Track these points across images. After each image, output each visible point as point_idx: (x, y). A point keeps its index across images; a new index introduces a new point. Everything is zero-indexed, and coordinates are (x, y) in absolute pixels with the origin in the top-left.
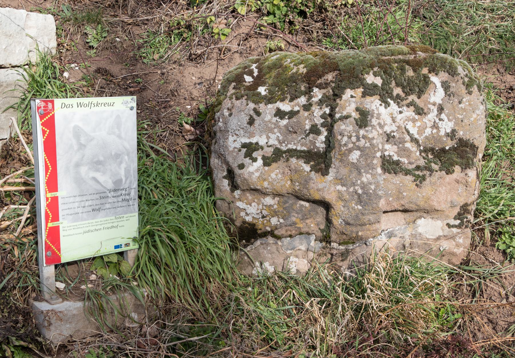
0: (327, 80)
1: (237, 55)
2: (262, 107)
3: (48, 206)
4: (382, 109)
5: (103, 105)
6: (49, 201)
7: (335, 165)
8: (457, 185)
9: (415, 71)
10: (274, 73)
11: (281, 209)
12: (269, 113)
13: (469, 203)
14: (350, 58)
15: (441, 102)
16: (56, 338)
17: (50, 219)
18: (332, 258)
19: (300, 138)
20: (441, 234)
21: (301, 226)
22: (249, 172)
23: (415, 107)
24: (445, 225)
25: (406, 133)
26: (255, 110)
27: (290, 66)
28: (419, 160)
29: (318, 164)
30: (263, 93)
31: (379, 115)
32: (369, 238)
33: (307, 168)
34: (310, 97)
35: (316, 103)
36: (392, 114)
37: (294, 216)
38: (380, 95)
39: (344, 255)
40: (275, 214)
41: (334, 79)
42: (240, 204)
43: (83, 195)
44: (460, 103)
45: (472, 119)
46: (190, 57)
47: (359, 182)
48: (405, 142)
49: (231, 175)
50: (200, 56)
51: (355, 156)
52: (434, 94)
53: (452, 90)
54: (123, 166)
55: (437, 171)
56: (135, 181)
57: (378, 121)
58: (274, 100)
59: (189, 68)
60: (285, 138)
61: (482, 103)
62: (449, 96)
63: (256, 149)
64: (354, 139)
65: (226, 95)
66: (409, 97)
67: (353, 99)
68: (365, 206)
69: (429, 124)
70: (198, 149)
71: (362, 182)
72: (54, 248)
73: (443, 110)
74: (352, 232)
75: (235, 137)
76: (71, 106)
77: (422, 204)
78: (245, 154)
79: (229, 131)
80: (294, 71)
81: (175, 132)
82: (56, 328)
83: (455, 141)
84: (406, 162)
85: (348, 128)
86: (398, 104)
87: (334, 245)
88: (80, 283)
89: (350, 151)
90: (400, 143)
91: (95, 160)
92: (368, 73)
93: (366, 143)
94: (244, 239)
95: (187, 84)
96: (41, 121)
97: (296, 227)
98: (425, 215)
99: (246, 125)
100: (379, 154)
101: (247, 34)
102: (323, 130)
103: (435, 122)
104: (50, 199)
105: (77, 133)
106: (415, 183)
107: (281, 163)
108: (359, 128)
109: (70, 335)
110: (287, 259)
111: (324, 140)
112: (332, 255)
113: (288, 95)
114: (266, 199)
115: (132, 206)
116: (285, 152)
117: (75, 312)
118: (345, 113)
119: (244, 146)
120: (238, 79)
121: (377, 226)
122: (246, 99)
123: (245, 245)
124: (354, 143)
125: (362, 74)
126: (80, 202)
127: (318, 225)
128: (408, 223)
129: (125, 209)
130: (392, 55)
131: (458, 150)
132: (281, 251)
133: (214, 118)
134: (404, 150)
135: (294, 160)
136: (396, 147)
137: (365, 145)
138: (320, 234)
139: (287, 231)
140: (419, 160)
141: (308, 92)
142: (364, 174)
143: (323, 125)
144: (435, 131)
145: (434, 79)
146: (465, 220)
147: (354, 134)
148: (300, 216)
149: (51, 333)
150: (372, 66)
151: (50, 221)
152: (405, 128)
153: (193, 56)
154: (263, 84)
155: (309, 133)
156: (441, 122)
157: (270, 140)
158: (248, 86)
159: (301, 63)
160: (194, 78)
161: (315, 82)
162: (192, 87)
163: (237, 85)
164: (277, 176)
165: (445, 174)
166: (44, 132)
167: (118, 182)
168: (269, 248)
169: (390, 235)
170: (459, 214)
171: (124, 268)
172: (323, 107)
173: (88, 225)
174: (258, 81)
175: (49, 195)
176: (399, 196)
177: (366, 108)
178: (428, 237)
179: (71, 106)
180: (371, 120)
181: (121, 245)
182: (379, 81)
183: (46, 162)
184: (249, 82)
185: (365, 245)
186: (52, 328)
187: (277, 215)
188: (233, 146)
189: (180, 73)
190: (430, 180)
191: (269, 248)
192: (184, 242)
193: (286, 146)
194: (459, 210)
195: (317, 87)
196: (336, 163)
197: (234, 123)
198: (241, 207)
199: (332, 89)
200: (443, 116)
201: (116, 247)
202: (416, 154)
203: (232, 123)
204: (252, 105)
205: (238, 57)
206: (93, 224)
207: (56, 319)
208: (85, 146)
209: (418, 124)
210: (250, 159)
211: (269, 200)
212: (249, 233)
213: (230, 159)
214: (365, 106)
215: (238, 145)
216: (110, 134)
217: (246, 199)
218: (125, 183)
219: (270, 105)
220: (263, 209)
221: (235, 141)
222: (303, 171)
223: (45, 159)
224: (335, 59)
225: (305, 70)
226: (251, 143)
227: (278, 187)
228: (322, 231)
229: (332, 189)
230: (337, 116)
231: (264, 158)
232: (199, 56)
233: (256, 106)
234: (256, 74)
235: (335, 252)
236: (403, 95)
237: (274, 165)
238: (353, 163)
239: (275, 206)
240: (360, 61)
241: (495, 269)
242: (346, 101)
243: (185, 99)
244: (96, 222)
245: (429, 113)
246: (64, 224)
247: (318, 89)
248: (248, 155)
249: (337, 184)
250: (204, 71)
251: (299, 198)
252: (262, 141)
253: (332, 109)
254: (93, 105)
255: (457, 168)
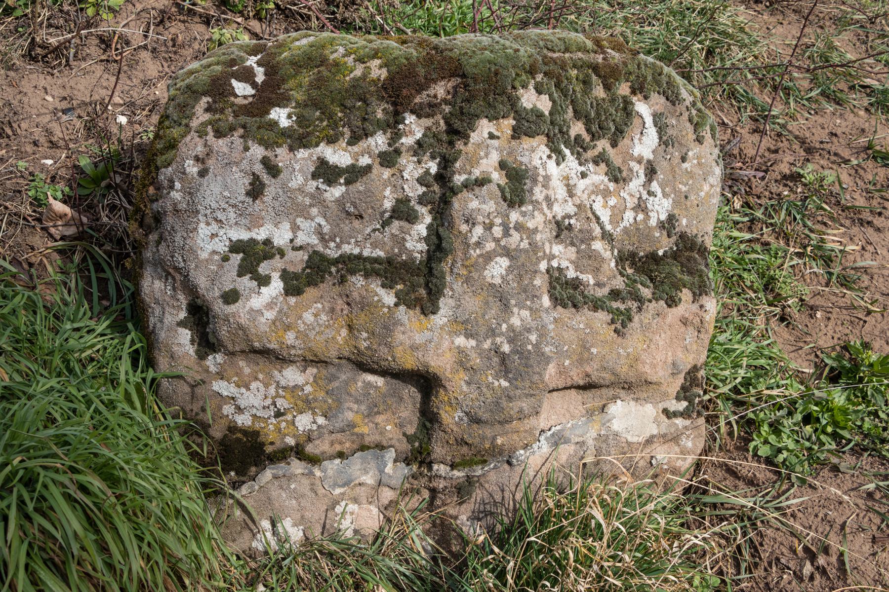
0: (435, 96)
1: (145, 55)
2: (282, 155)
4: (551, 164)
7: (452, 289)
8: (683, 329)
9: (607, 87)
10: (306, 78)
11: (321, 395)
12: (300, 171)
13: (699, 365)
14: (486, 49)
15: (651, 157)
18: (433, 498)
19: (369, 230)
20: (655, 432)
21: (365, 430)
22: (252, 310)
23: (608, 165)
24: (660, 411)
25: (594, 219)
26: (265, 162)
27: (346, 63)
28: (615, 277)
29: (413, 288)
30: (284, 123)
31: (547, 178)
32: (516, 449)
33: (389, 298)
34: (396, 136)
35: (410, 148)
36: (567, 178)
37: (350, 409)
38: (547, 135)
39: (463, 491)
40: (307, 405)
41: (450, 97)
42: (222, 387)
44: (684, 159)
45: (702, 194)
46: (30, 51)
47: (504, 326)
48: (593, 239)
49: (199, 316)
50: (58, 51)
51: (498, 269)
52: (640, 139)
53: (670, 132)
55: (650, 301)
57: (545, 191)
58: (314, 140)
59: (31, 76)
60: (336, 230)
61: (717, 162)
62: (666, 144)
63: (268, 256)
64: (497, 231)
65: (187, 125)
66: (598, 143)
67: (495, 142)
68: (516, 380)
69: (631, 202)
70: (84, 260)
71: (511, 328)
73: (655, 173)
74: (483, 438)
75: (214, 227)
77: (623, 370)
78: (240, 266)
79: (198, 212)
80: (358, 72)
81: (24, 219)
83: (674, 238)
84: (592, 282)
85: (484, 206)
86: (579, 156)
87: (441, 469)
89: (488, 258)
90: (582, 242)
92: (525, 86)
93: (522, 240)
94: (232, 470)
95: (34, 111)
97: (352, 434)
98: (622, 393)
99: (242, 198)
100: (543, 266)
101: (163, 12)
102: (423, 210)
103: (640, 198)
106: (613, 327)
107: (327, 287)
108: (509, 206)
110: (333, 509)
111: (424, 233)
112: (433, 492)
113: (346, 129)
114: (285, 372)
116: (336, 262)
118: (477, 173)
119: (236, 247)
120: (219, 90)
121: (533, 421)
122: (242, 137)
123: (234, 483)
124: (497, 241)
125: (514, 87)
127: (401, 426)
128: (590, 413)
130: (567, 50)
131: (680, 256)
132: (321, 491)
133: (154, 182)
134: (590, 257)
135: (358, 281)
136: (574, 249)
137: (519, 245)
138: (405, 446)
139: (332, 444)
140: (615, 277)
141: (393, 125)
142: (515, 310)
143: (421, 200)
144: (640, 217)
145: (642, 108)
146: (697, 400)
147: (498, 221)
148: (363, 408)
150: (532, 72)
152: (591, 208)
153: (39, 50)
154: (282, 101)
155: (391, 217)
156: (651, 198)
157: (300, 234)
158: (241, 107)
159: (375, 56)
160: (49, 98)
161: (410, 97)
162: (48, 118)
163: (215, 102)
164: (316, 318)
165: (665, 305)
168: (293, 486)
169: (558, 441)
170: (683, 388)
172: (425, 158)
174: (270, 94)
176: (583, 355)
177: (521, 163)
178: (630, 439)
180: (532, 189)
182: (544, 104)
184: (245, 97)
185: (506, 466)
187: (310, 408)
188: (210, 248)
189: (11, 85)
190: (641, 320)
191: (293, 486)
192: (118, 492)
193: (338, 247)
194: (683, 381)
195: (413, 112)
196: (455, 287)
197: (212, 191)
198: (225, 393)
199: (443, 118)
200: (655, 186)
202: (609, 265)
203: (208, 192)
204: (258, 151)
205: (149, 59)
209: (612, 201)
210: (251, 279)
211: (292, 376)
212: (244, 453)
213: (201, 281)
214: (519, 158)
215: (222, 247)
217: (237, 374)
219: (302, 150)
220: (278, 396)
221: (213, 236)
222: (380, 304)
224: (451, 50)
225: (384, 73)
226: (253, 241)
227: (318, 342)
228: (409, 439)
229: (446, 344)
230: (459, 179)
231: (285, 276)
232: (53, 52)
233: (269, 154)
234: (260, 78)
235: (441, 484)
236: (587, 138)
237: (311, 293)
238: (492, 285)
239: (308, 389)
240: (507, 57)
241: (768, 498)
242: (479, 145)
243: (35, 143)
245: (631, 180)
247: (414, 117)
248: (249, 268)
249: (457, 334)
250: (72, 83)
251: (363, 367)
252: (281, 236)
253: (446, 163)
255: (686, 295)
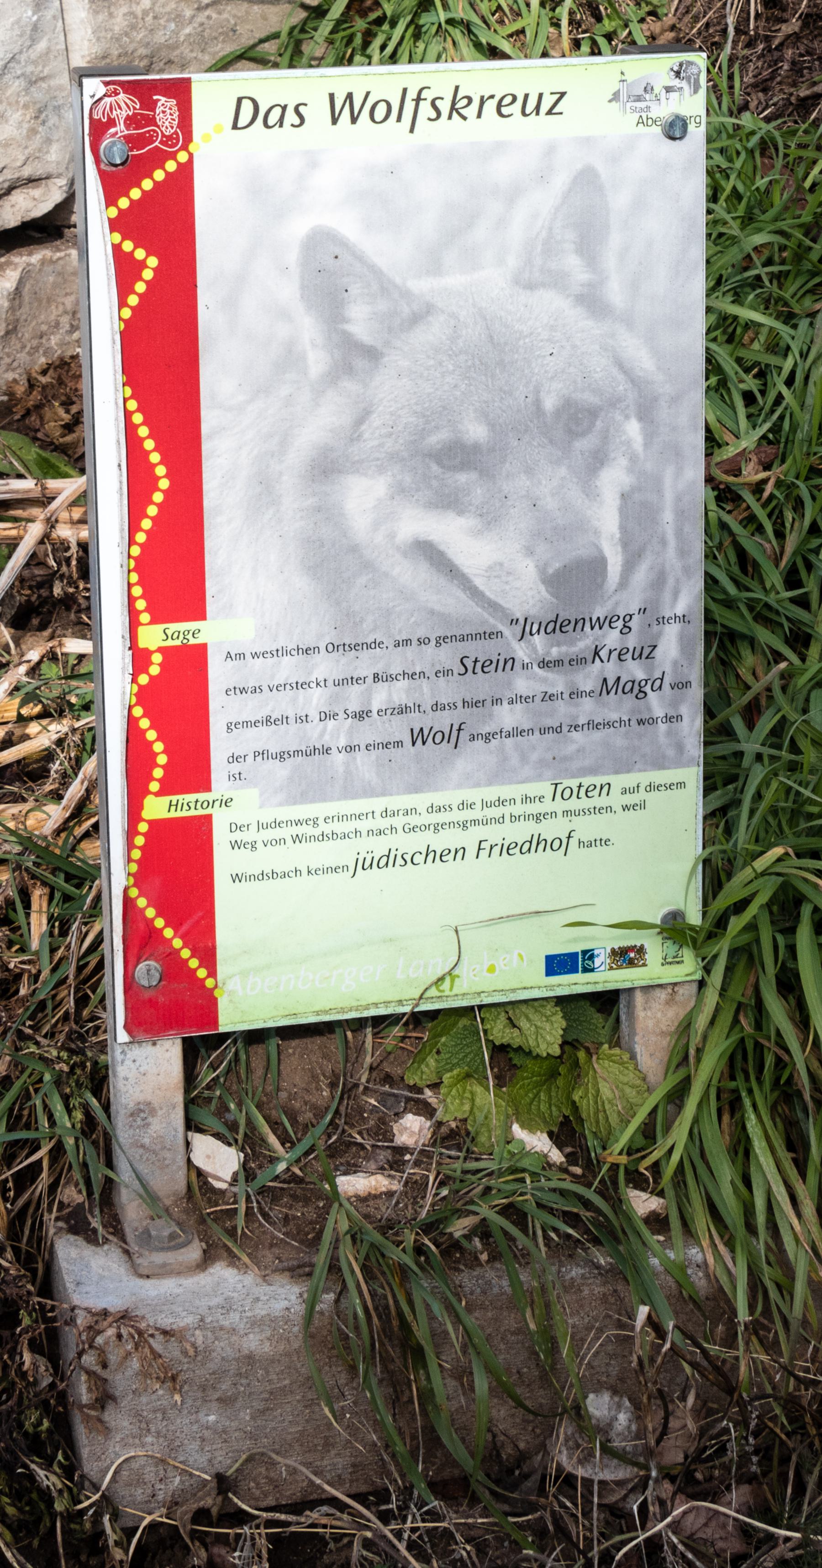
3: (143, 696)
5: (490, 106)
6: (155, 670)
16: (140, 1481)
17: (158, 773)
43: (355, 647)
54: (614, 479)
56: (687, 570)
72: (177, 943)
76: (291, 117)
82: (143, 1425)
88: (333, 1152)
91: (435, 439)
96: (111, 201)
104: (157, 658)
105: (329, 273)
109: (220, 1478)
115: (662, 727)
117: (254, 1343)
126: (337, 684)
129: (618, 738)
149: (113, 1446)
151: (154, 786)
166: (126, 270)
167: (575, 579)
171: (606, 1091)
173: (384, 823)
175: (152, 636)
179: (291, 117)
181: (589, 955)
183: (130, 429)
186: (115, 1417)
201: (557, 964)
206: (414, 820)
207: (144, 1374)
208: (372, 354)
216: (530, 286)
218: (624, 583)
223: (128, 415)
244: (431, 809)
246: (238, 808)
254: (426, 109)
